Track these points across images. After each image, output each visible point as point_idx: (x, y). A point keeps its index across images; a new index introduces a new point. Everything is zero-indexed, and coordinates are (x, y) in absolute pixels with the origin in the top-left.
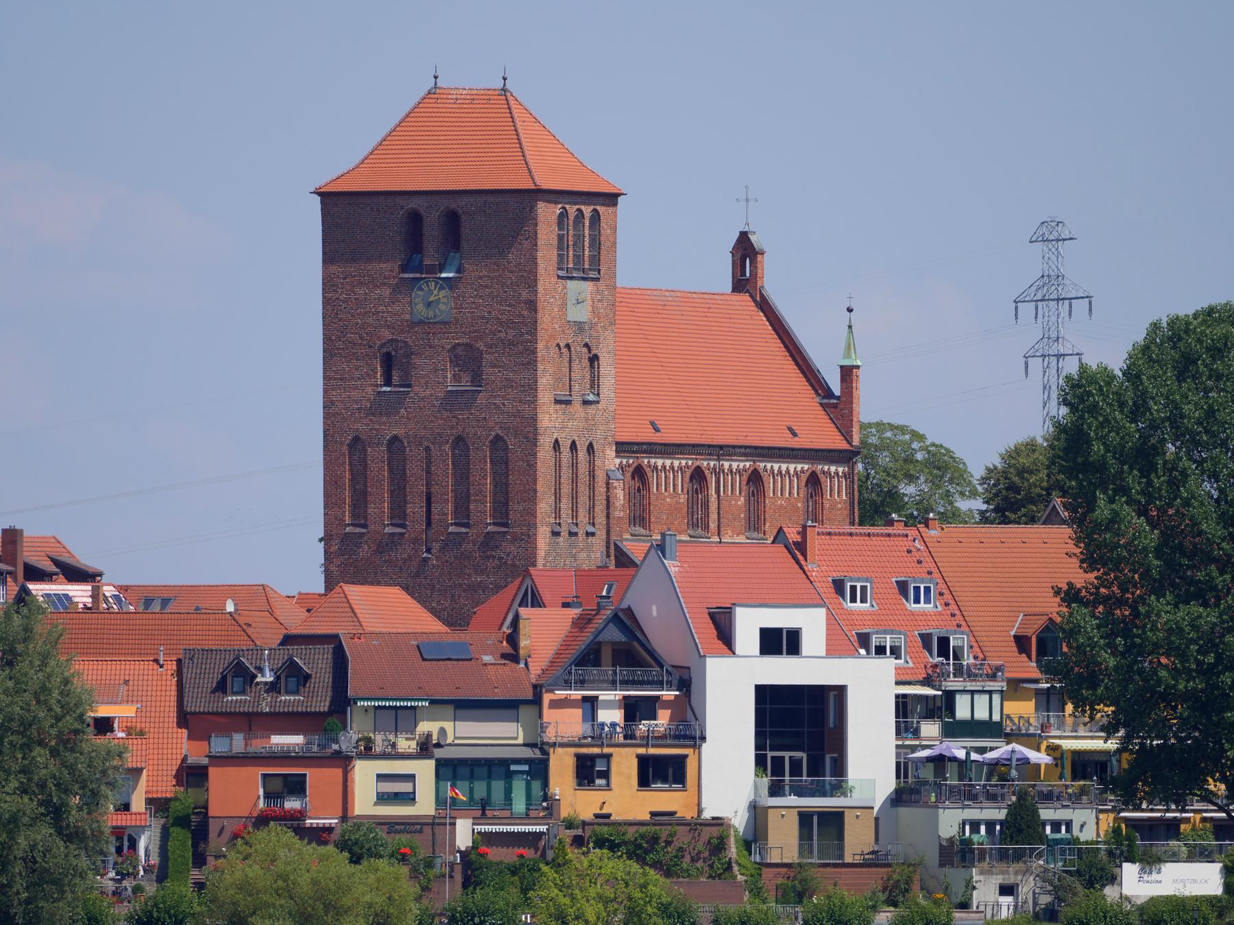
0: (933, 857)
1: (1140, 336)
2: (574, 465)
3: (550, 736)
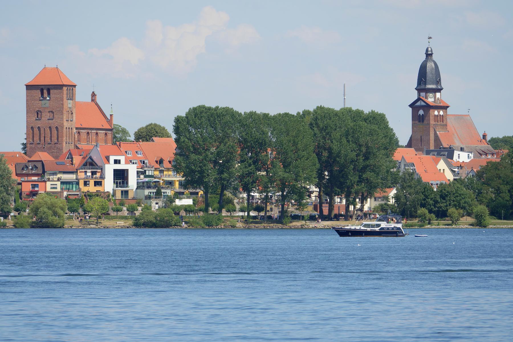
0: (144, 198)
1: (187, 111)
2: (69, 131)
3: (79, 178)
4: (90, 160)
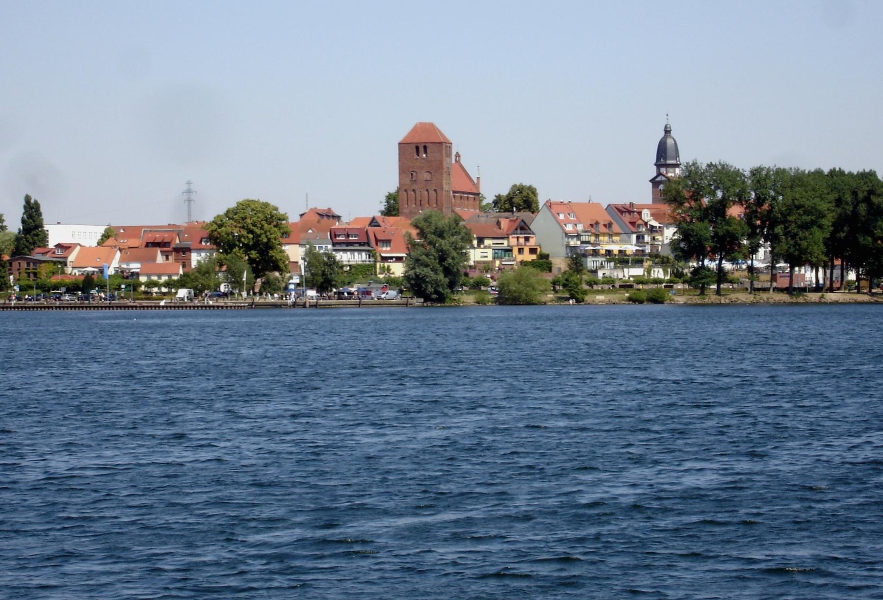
4: (523, 224)
